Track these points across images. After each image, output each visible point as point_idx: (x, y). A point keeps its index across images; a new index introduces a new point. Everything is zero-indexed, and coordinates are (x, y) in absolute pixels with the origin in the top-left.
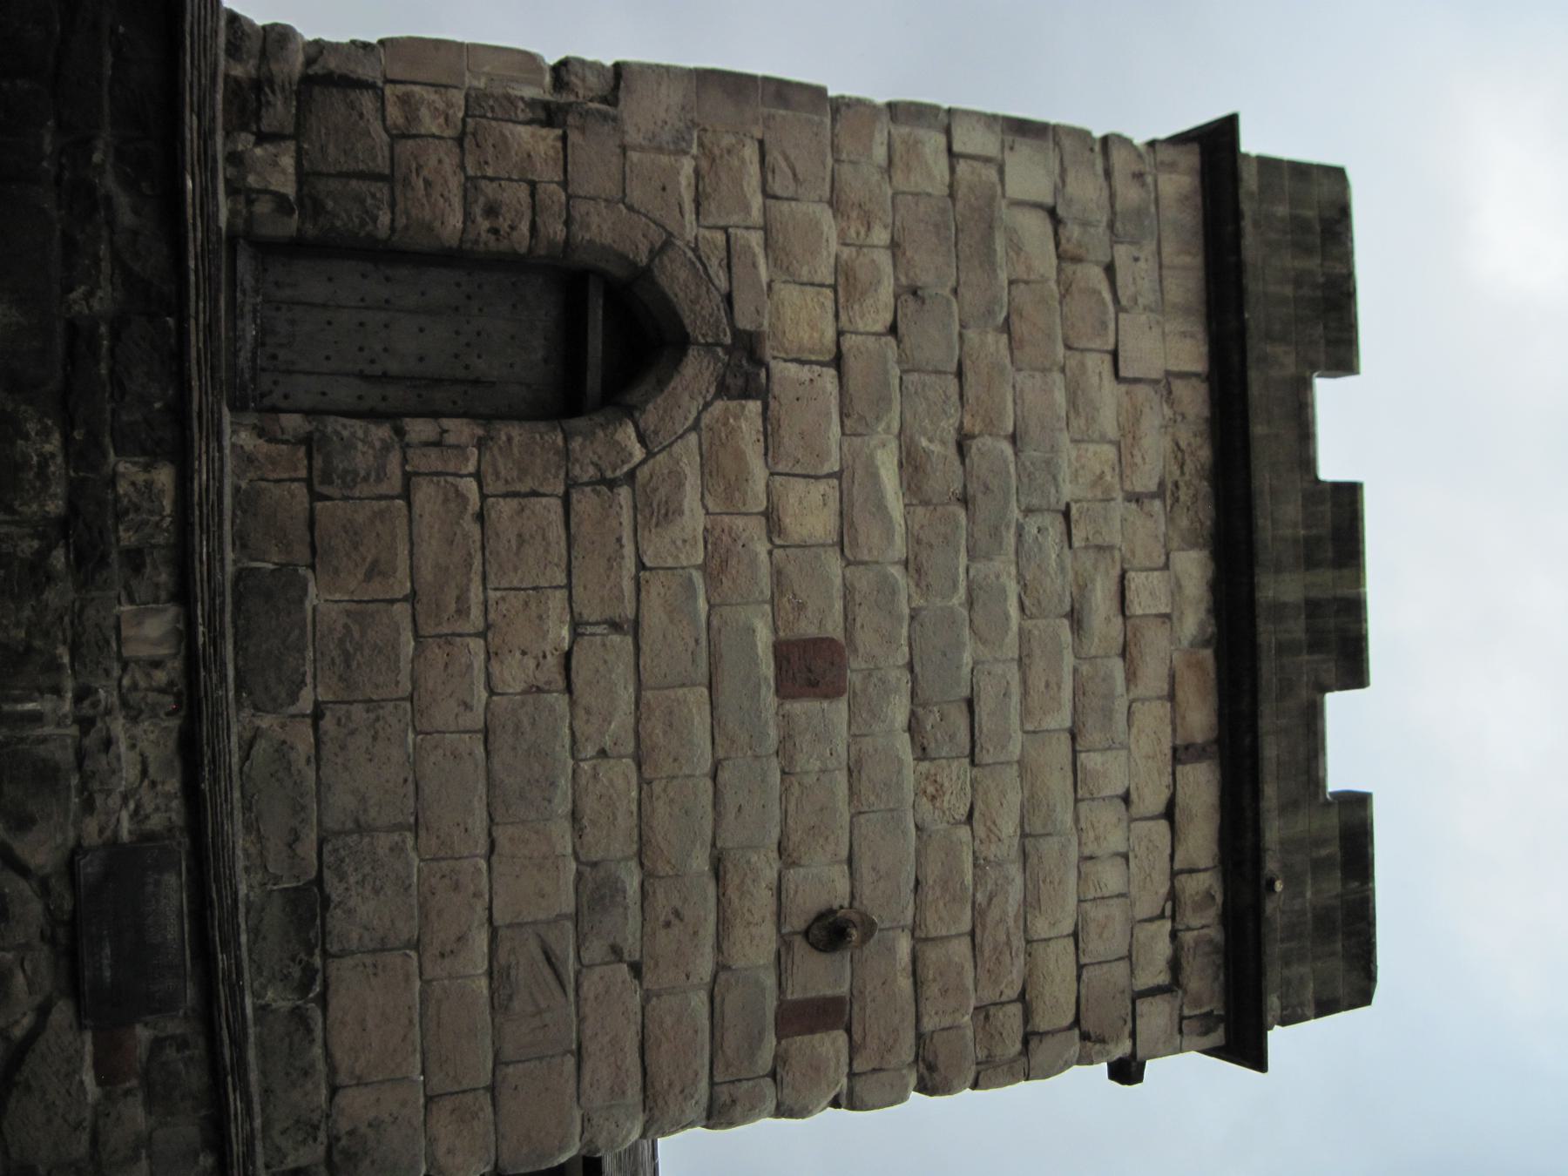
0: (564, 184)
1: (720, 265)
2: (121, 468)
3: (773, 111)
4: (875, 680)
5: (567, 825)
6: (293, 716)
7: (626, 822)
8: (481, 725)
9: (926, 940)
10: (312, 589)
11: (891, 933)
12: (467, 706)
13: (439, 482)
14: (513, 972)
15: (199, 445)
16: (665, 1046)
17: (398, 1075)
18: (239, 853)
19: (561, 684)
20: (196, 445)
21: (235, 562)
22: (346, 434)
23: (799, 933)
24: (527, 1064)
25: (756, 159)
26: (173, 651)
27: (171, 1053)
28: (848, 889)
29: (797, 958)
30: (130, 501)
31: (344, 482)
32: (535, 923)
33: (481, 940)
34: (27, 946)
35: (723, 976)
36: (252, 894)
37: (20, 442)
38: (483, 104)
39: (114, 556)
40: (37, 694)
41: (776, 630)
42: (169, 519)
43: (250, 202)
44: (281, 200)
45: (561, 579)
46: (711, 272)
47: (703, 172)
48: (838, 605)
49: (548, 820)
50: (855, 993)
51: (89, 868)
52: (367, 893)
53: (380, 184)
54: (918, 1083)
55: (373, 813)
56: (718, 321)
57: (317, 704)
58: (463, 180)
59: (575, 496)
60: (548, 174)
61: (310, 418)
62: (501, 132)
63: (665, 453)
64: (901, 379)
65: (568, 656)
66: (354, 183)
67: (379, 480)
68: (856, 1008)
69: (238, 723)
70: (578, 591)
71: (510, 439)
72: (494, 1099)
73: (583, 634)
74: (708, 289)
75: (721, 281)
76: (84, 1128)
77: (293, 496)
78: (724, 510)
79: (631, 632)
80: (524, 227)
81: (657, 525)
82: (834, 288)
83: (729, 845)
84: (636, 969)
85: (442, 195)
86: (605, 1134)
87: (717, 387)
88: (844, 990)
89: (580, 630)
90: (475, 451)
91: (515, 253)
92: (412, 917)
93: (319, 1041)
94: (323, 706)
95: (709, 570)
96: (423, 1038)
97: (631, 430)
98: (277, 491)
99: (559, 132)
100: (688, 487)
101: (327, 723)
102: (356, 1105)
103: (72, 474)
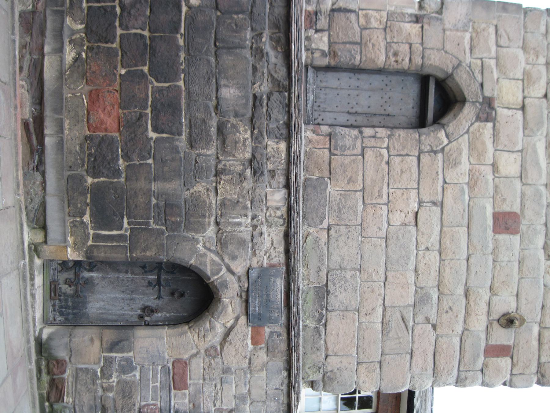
0: (422, 44)
1: (479, 72)
2: (269, 143)
3: (501, 14)
4: (531, 229)
5: (413, 273)
6: (321, 229)
7: (434, 274)
8: (385, 236)
9: (545, 328)
10: (329, 186)
11: (531, 324)
12: (380, 229)
13: (374, 150)
14: (390, 323)
15: (294, 135)
16: (443, 355)
17: (348, 354)
18: (301, 273)
19: (413, 223)
20: (293, 135)
21: (304, 176)
22: (343, 133)
23: (495, 320)
24: (393, 355)
25: (494, 32)
26: (283, 205)
27: (275, 337)
28: (515, 306)
29: (494, 329)
30: (271, 154)
31: (341, 149)
32: (399, 306)
33: (380, 310)
34: (233, 297)
35: (466, 333)
36: (304, 288)
37: (237, 134)
38: (393, 16)
39: (266, 172)
40: (240, 217)
41: (494, 208)
42: (284, 160)
43: (312, 53)
44: (323, 54)
45: (416, 186)
46: (476, 75)
47: (473, 38)
48: (519, 200)
49: (406, 271)
50: (516, 344)
51: (254, 274)
52: (342, 291)
53: (357, 46)
54: (537, 381)
55: (346, 263)
56: (477, 93)
57: (329, 225)
58: (386, 43)
59: (422, 156)
60: (416, 40)
61: (331, 127)
62: (399, 26)
63: (455, 142)
64: (548, 115)
65: (417, 213)
66: (348, 46)
67: (353, 149)
68: (515, 350)
69: (303, 229)
70: (421, 190)
71: (399, 136)
72: (380, 366)
73: (423, 206)
74: (474, 82)
75: (479, 78)
76: (247, 358)
77: (324, 154)
78: (477, 163)
79: (440, 205)
80: (407, 60)
81: (451, 168)
82: (523, 80)
83: (472, 285)
84: (434, 327)
85: (378, 49)
86: (418, 383)
87: (476, 117)
88: (511, 343)
89: (421, 204)
90: (387, 139)
91: (404, 69)
92: (357, 300)
93: (323, 339)
94: (331, 226)
95: (470, 185)
96: (358, 342)
97: (443, 133)
98: (319, 152)
99: (420, 25)
100: (463, 154)
101: (332, 232)
102: (333, 362)
103: (253, 144)
